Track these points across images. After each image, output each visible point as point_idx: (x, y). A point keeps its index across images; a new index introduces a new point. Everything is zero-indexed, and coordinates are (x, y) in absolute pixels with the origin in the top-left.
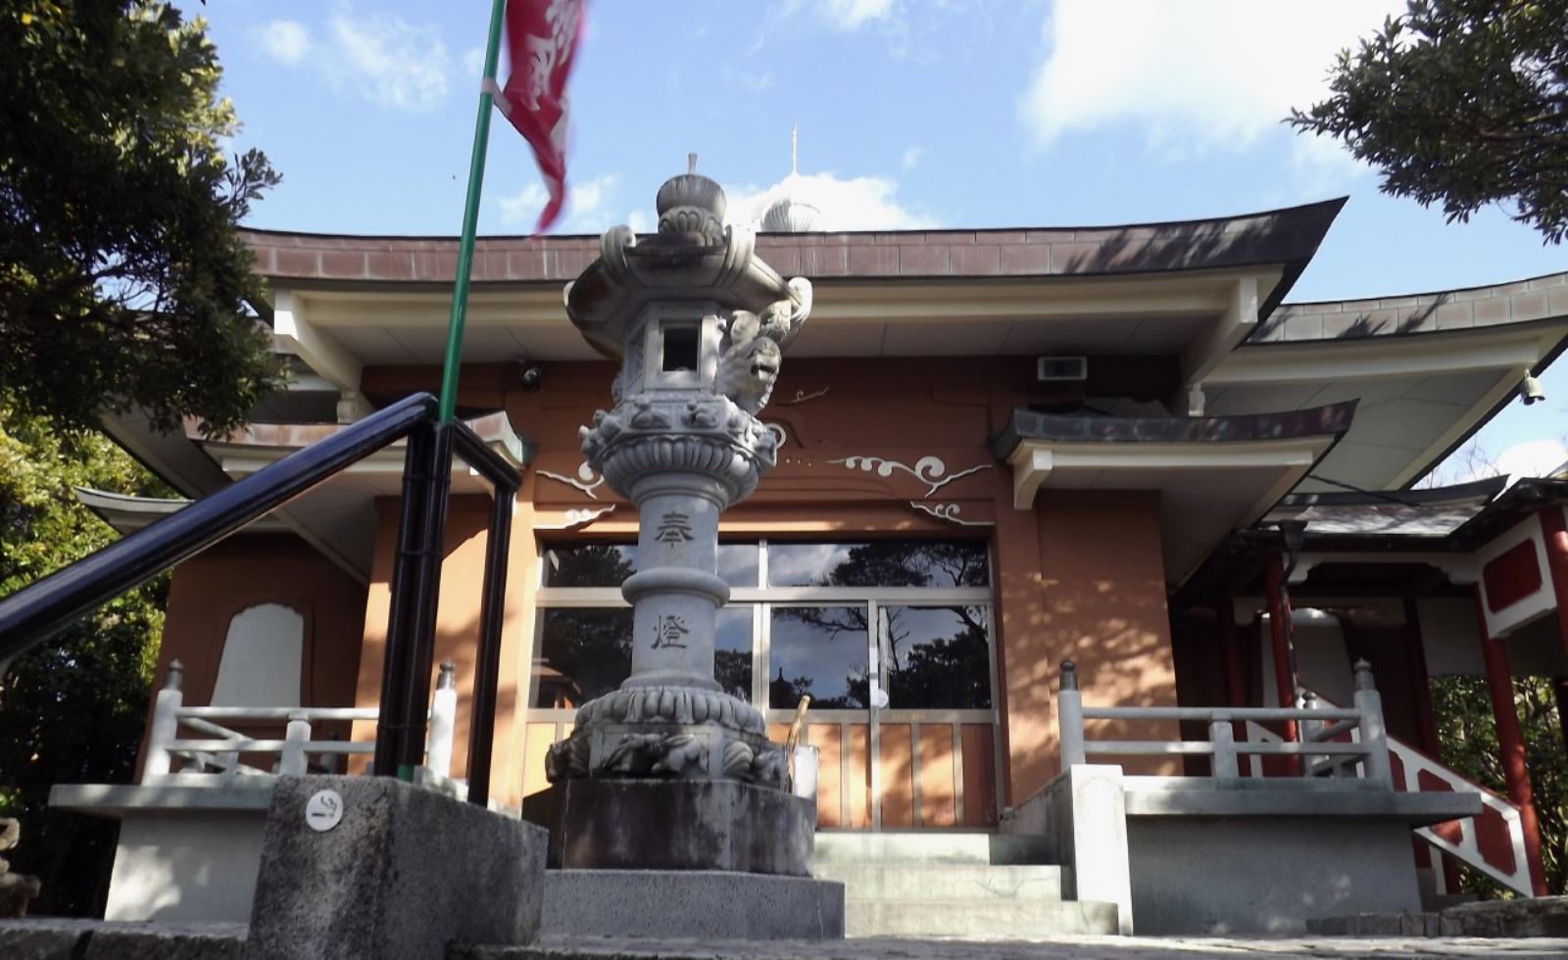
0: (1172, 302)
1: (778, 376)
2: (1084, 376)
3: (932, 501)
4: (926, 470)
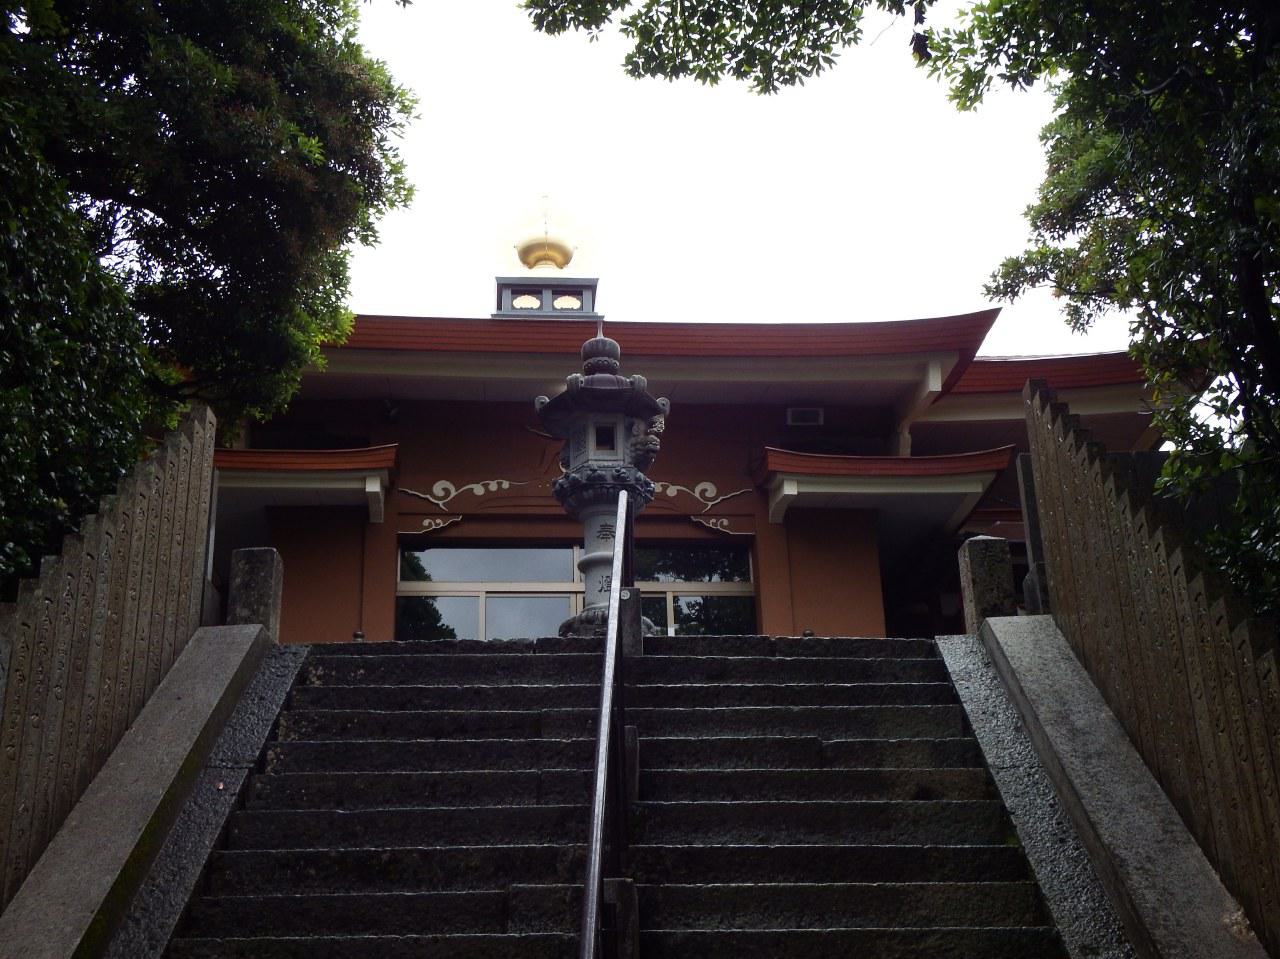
0: (895, 374)
1: (180, 402)
2: (821, 421)
3: (708, 515)
4: (703, 492)
